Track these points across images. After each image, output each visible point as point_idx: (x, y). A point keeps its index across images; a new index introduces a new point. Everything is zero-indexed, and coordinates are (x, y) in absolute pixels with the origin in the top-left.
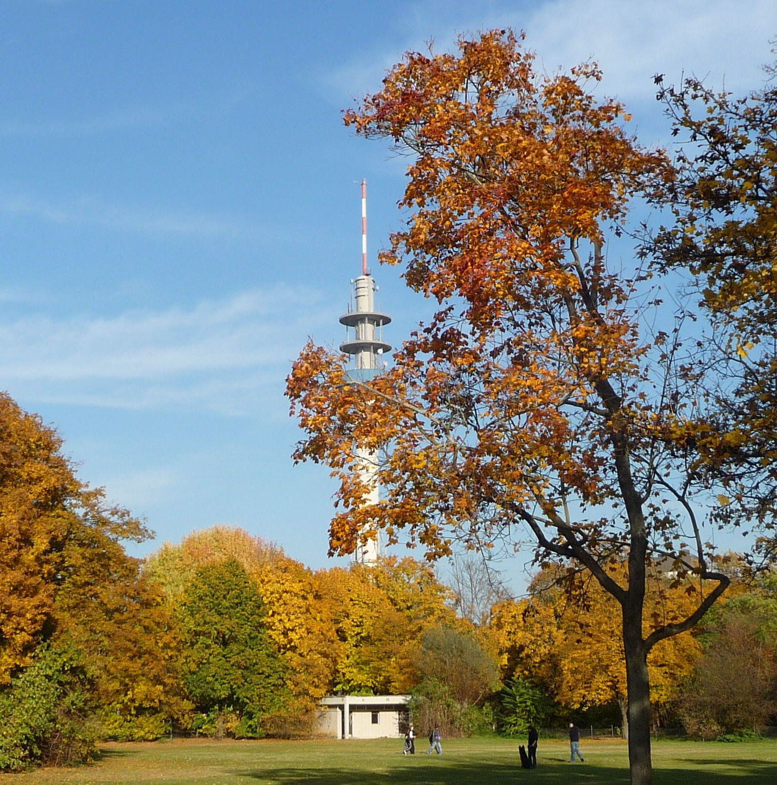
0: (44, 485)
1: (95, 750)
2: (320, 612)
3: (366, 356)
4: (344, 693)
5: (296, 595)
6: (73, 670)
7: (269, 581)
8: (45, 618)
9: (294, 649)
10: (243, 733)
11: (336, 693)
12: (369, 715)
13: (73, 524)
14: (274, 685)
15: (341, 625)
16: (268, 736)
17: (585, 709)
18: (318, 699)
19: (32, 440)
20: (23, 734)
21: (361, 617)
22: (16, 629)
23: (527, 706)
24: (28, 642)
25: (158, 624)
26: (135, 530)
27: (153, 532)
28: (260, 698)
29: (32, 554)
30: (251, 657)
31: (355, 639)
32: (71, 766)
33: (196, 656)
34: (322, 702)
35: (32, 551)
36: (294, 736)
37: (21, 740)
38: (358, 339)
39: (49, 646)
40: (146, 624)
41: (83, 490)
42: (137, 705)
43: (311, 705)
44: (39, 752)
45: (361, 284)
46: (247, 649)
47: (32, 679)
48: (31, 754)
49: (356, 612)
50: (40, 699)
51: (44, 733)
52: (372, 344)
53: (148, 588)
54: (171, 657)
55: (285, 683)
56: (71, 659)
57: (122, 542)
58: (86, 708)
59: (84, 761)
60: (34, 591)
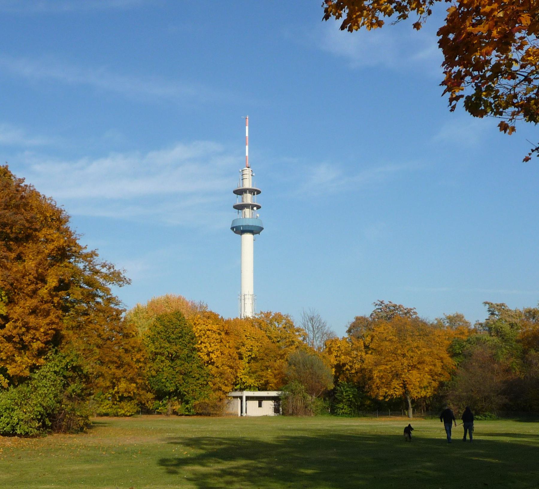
0: (56, 244)
1: (89, 422)
2: (228, 342)
3: (247, 211)
4: (242, 390)
5: (214, 332)
6: (74, 369)
7: (199, 324)
8: (54, 332)
9: (213, 363)
10: (183, 412)
11: (236, 390)
12: (257, 402)
13: (77, 273)
14: (201, 384)
15: (240, 350)
16: (198, 414)
17: (387, 400)
18: (227, 393)
20: (38, 411)
21: (252, 346)
22: (33, 338)
23: (349, 398)
24: (42, 348)
25: (133, 348)
26: (117, 277)
27: (130, 280)
28: (193, 391)
29: (47, 289)
30: (188, 368)
31: (247, 359)
32: (72, 433)
33: (156, 367)
34: (230, 394)
35: (46, 287)
36: (213, 414)
37: (37, 416)
38: (243, 201)
39: (56, 351)
40: (126, 347)
41: (85, 251)
42: (120, 395)
43: (223, 396)
44: (50, 424)
45: (245, 172)
46: (186, 363)
47: (45, 374)
48: (44, 425)
49: (249, 343)
50: (50, 387)
51: (53, 410)
52: (251, 204)
53: (127, 327)
54: (141, 367)
55: (207, 383)
56: (72, 360)
57: (109, 286)
58: (83, 394)
59: (81, 430)
60: (47, 314)
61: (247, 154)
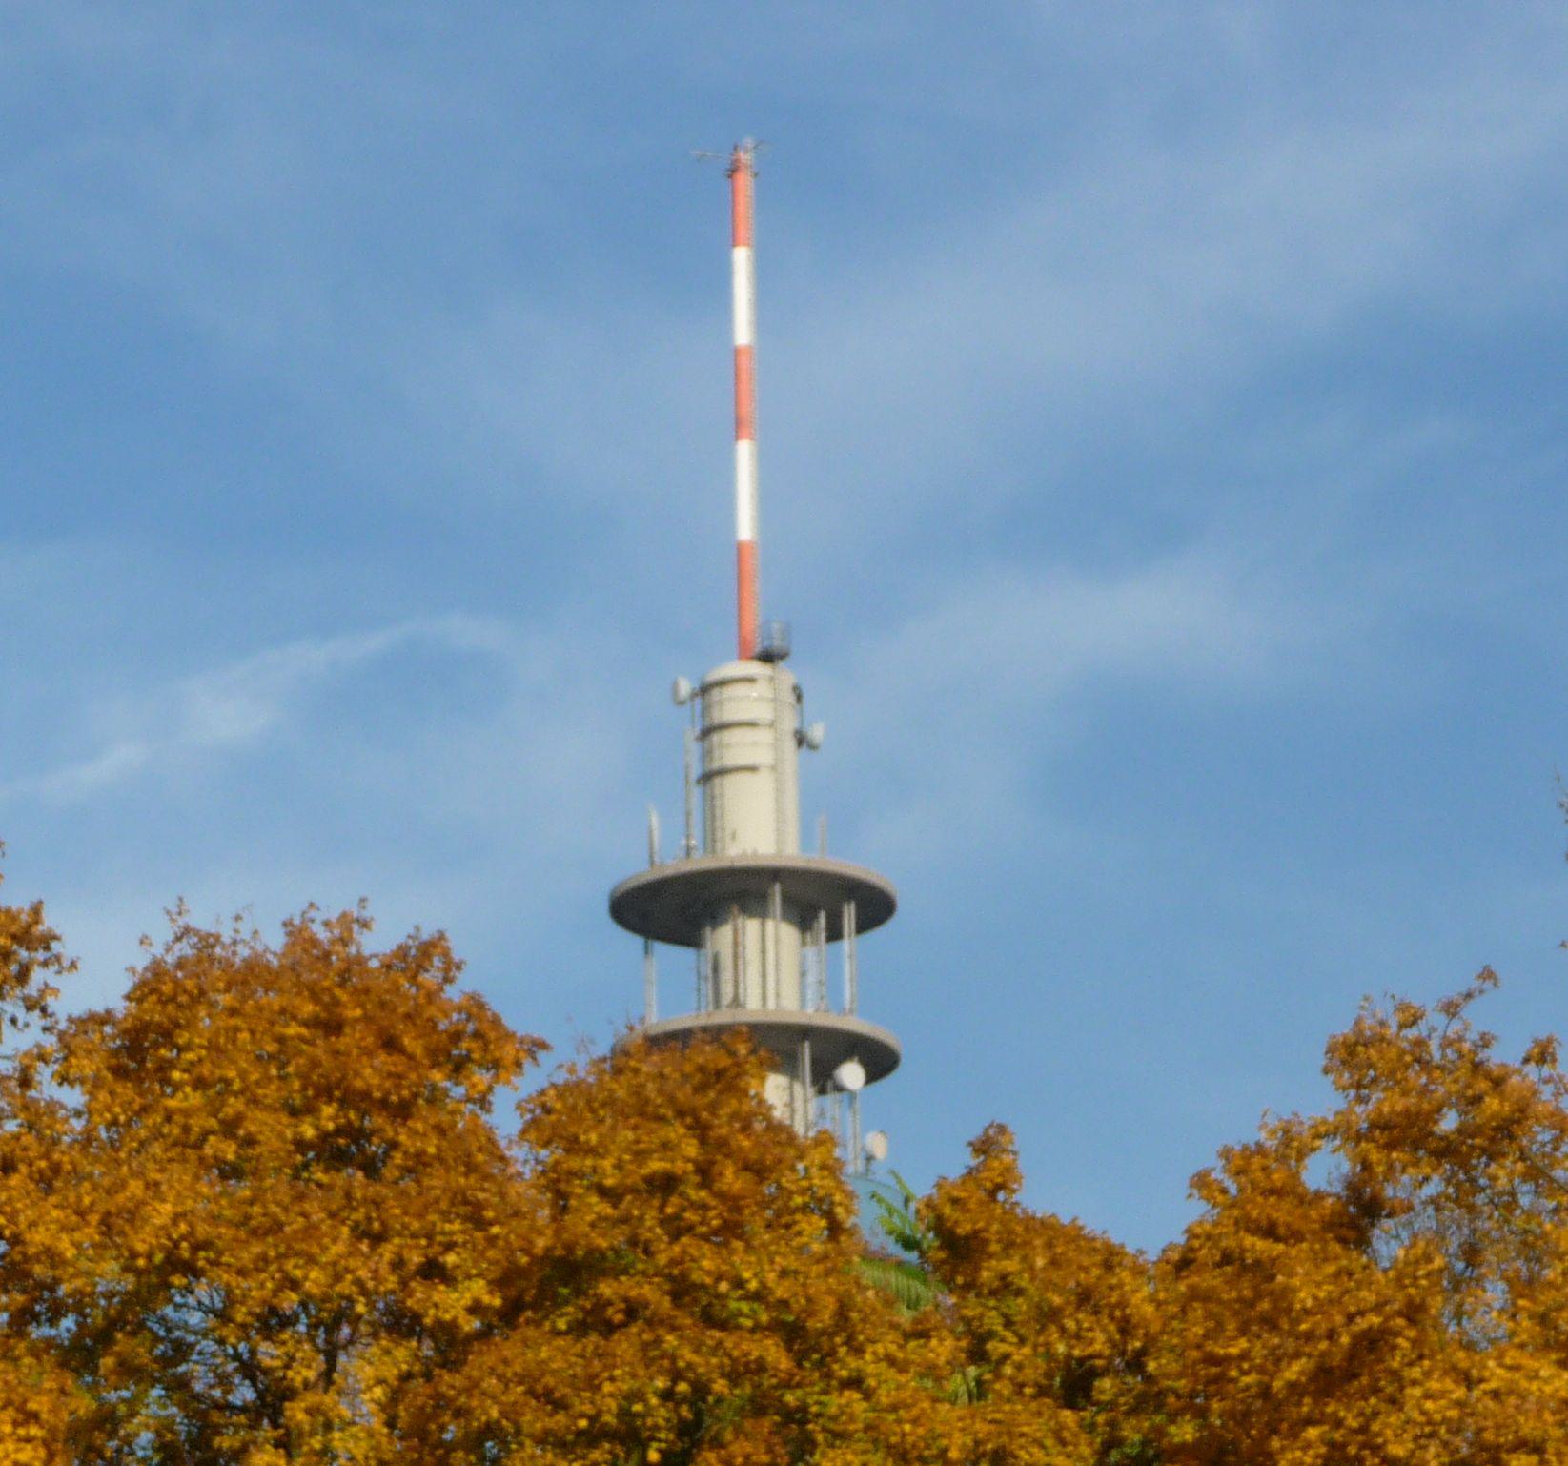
19: (1061, 1348)
45: (735, 704)
52: (805, 1032)
61: (743, 333)
